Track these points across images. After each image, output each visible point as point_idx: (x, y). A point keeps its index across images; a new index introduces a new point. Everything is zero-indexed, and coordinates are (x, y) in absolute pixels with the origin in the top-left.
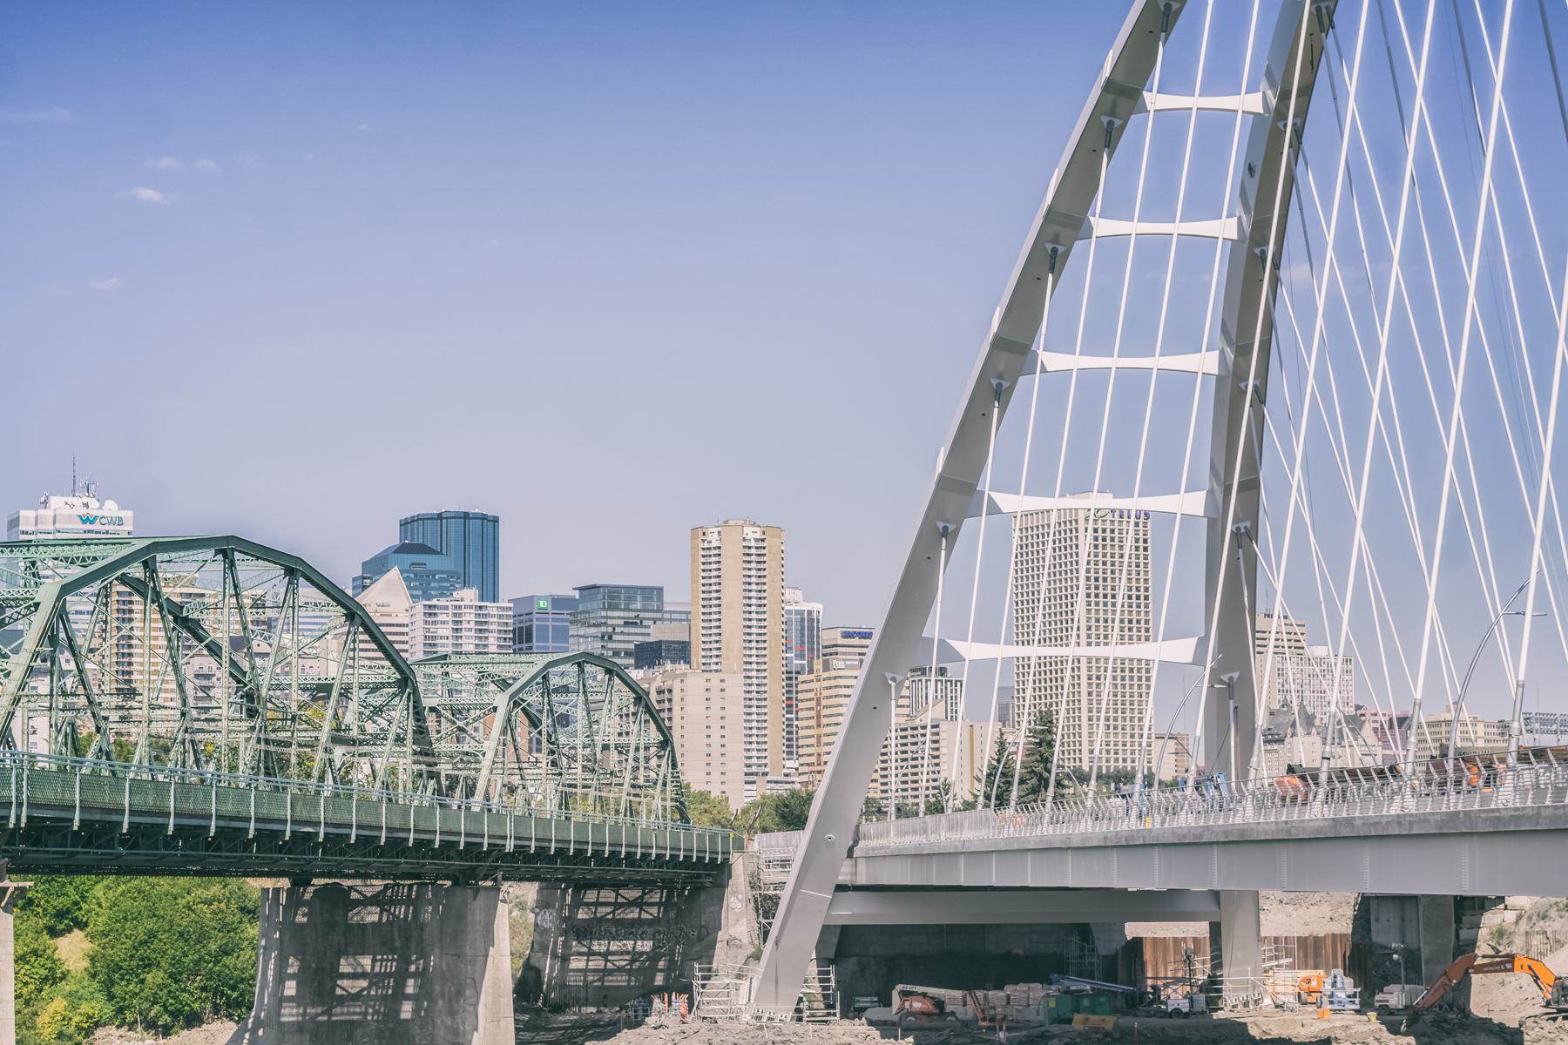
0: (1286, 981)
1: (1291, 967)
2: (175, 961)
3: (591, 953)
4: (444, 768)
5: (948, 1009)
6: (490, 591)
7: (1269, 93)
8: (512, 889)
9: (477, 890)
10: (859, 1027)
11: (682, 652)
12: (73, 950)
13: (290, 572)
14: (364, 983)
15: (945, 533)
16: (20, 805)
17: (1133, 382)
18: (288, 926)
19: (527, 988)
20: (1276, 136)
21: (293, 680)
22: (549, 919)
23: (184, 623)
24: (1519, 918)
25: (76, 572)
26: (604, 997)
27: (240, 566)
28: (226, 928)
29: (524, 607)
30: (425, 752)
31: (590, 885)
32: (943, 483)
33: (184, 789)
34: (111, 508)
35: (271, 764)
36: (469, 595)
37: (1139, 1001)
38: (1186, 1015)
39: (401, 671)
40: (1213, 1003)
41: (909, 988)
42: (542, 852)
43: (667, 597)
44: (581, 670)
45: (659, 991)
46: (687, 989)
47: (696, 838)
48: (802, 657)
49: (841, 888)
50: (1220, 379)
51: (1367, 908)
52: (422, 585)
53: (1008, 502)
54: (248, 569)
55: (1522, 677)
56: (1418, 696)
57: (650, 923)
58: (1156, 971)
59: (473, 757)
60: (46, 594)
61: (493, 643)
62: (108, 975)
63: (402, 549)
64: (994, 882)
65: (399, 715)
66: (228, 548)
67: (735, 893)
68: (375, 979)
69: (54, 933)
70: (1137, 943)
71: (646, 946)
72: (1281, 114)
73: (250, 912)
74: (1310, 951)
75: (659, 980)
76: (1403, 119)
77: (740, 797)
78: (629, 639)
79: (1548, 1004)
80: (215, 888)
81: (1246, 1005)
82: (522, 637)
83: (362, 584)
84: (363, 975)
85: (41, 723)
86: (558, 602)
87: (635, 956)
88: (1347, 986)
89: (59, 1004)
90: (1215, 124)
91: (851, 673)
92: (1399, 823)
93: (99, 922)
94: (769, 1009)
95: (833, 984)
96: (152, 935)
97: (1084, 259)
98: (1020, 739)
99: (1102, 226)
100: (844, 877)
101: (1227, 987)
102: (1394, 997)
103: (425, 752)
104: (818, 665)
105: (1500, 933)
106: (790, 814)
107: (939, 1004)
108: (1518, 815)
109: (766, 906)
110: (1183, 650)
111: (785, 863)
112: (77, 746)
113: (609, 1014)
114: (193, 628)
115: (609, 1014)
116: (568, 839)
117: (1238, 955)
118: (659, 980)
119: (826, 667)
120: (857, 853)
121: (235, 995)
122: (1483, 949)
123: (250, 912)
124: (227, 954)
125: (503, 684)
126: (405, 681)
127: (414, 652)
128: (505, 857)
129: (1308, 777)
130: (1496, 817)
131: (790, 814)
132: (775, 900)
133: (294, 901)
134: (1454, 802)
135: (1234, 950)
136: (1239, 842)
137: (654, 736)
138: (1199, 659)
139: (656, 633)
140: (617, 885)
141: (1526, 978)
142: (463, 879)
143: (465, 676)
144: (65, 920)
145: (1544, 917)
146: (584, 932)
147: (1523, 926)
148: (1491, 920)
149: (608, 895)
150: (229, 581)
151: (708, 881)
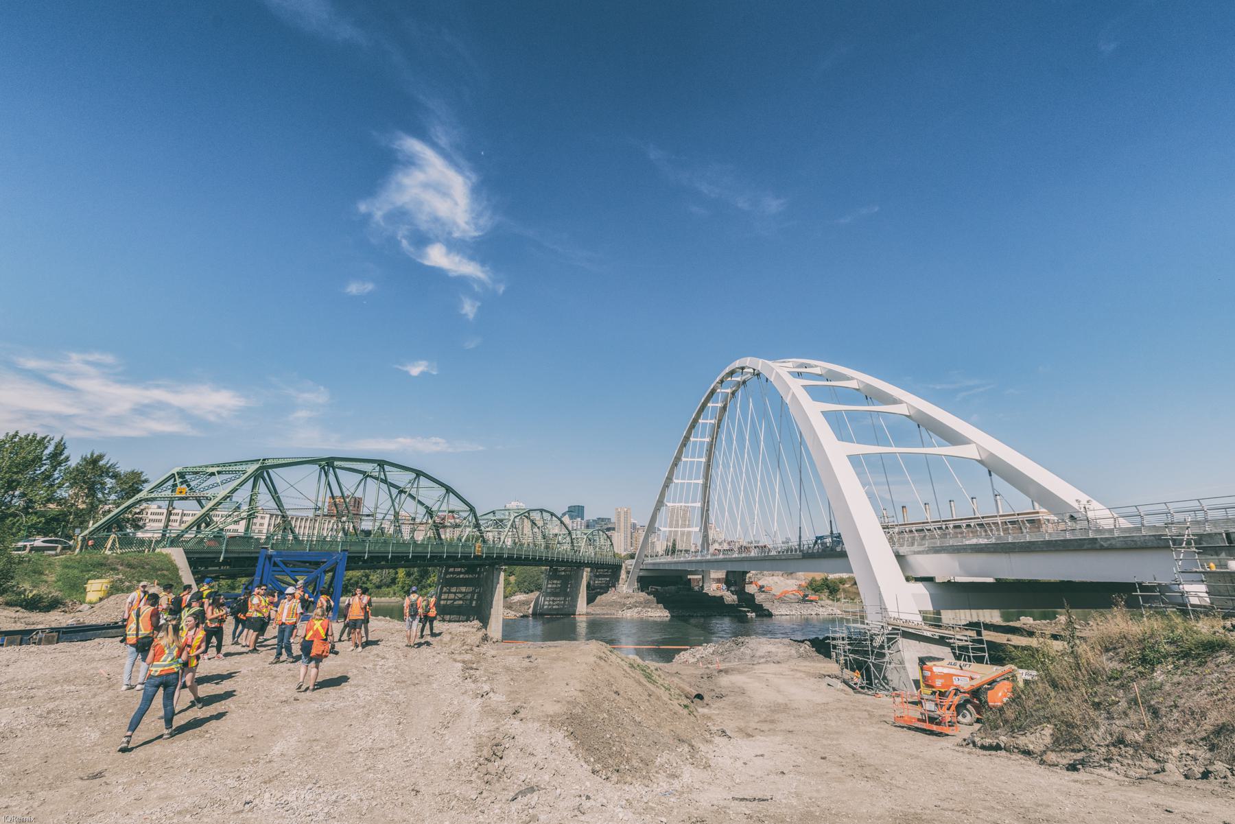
0: (714, 586)
4: (575, 548)
6: (582, 519)
8: (586, 569)
10: (644, 593)
11: (614, 529)
12: (512, 579)
13: (552, 515)
17: (689, 484)
18: (549, 575)
19: (588, 586)
20: (711, 445)
21: (551, 533)
22: (592, 574)
23: (534, 523)
25: (517, 514)
26: (601, 588)
29: (588, 522)
30: (573, 546)
32: (658, 501)
33: (533, 552)
34: (521, 504)
35: (547, 547)
36: (579, 519)
37: (691, 589)
40: (703, 589)
42: (567, 561)
44: (542, 514)
46: (615, 587)
47: (617, 561)
49: (641, 569)
50: (703, 484)
51: (728, 573)
52: (571, 517)
53: (668, 504)
54: (544, 514)
59: (580, 547)
60: (512, 518)
61: (583, 527)
62: (518, 584)
63: (568, 511)
64: (673, 568)
65: (568, 539)
66: (542, 511)
69: (509, 576)
70: (690, 579)
71: (608, 579)
72: (712, 441)
73: (542, 573)
74: (718, 581)
76: (732, 443)
77: (624, 554)
78: (606, 527)
80: (536, 568)
82: (588, 526)
83: (562, 517)
85: (510, 540)
86: (593, 520)
87: (606, 581)
88: (725, 587)
89: (510, 588)
90: (702, 443)
91: (642, 534)
93: (517, 574)
97: (681, 464)
98: (670, 544)
99: (684, 459)
101: (705, 587)
102: (733, 589)
103: (573, 546)
105: (750, 578)
106: (632, 556)
108: (755, 557)
109: (628, 572)
110: (697, 529)
111: (631, 565)
112: (515, 543)
113: (602, 591)
114: (535, 524)
115: (602, 591)
116: (457, 551)
122: (747, 580)
123: (542, 573)
125: (585, 534)
126: (570, 533)
127: (570, 529)
128: (585, 564)
129: (719, 551)
130: (751, 557)
131: (632, 556)
132: (630, 572)
133: (550, 571)
134: (743, 555)
135: (706, 581)
136: (708, 562)
137: (609, 543)
138: (700, 530)
139: (609, 526)
141: (755, 585)
142: (492, 565)
143: (578, 532)
144: (511, 574)
146: (597, 577)
148: (748, 575)
149: (602, 570)
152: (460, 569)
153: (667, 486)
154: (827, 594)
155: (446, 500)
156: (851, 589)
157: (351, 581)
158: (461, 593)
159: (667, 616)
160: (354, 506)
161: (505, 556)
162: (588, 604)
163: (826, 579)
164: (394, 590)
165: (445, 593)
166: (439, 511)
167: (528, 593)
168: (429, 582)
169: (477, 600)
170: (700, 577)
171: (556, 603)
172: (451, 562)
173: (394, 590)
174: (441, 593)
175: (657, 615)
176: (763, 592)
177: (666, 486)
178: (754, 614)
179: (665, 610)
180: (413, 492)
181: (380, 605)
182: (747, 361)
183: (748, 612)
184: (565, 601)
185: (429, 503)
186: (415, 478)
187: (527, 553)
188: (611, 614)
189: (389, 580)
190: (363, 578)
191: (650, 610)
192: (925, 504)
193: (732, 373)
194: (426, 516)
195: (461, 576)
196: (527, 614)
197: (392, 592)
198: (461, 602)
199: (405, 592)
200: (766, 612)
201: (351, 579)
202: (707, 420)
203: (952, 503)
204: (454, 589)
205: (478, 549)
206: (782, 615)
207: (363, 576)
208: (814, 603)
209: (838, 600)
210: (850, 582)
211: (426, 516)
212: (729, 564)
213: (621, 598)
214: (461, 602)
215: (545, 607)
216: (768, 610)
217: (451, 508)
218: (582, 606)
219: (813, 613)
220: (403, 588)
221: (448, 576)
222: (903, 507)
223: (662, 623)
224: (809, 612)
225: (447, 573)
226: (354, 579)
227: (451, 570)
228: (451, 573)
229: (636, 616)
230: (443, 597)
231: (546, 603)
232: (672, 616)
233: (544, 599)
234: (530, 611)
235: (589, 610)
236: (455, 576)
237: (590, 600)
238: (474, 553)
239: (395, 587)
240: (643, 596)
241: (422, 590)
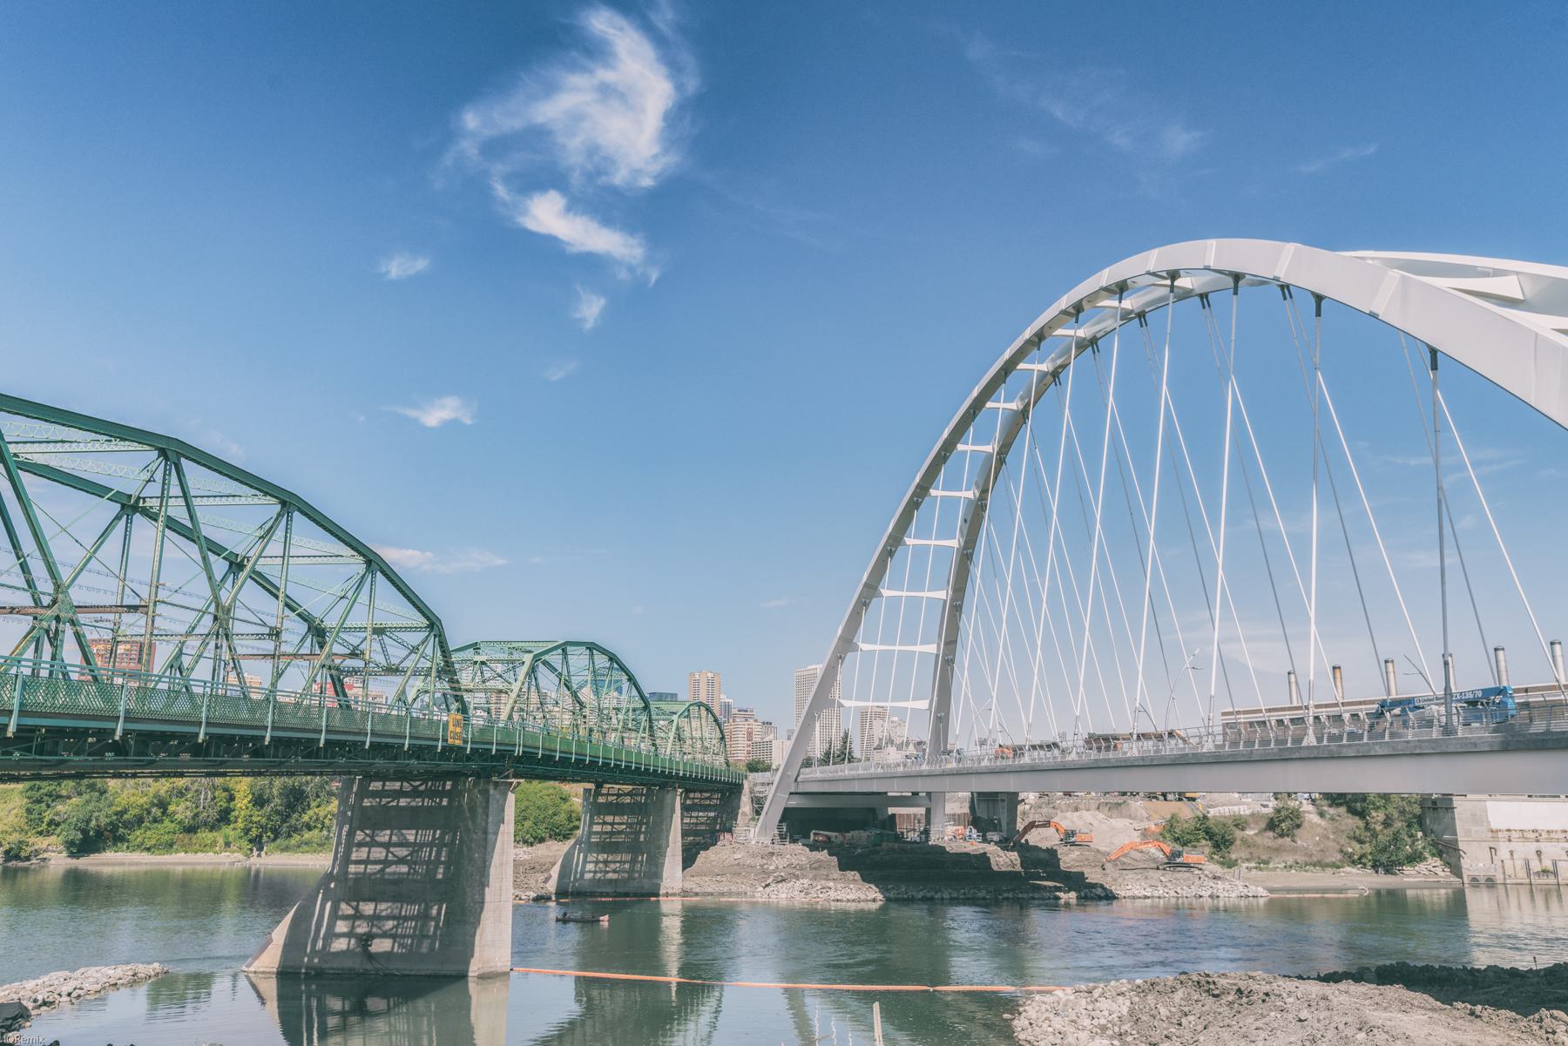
0: (951, 829)
1: (954, 825)
2: (536, 818)
3: (691, 817)
5: (832, 840)
7: (976, 491)
9: (668, 791)
10: (798, 847)
14: (624, 827)
15: (840, 657)
16: (520, 746)
24: (1031, 808)
27: (595, 657)
28: (555, 805)
31: (691, 792)
38: (918, 843)
39: (645, 703)
41: (817, 832)
43: (679, 696)
45: (718, 831)
48: (725, 717)
49: (791, 794)
55: (1030, 721)
56: (1078, 714)
57: (713, 806)
58: (901, 827)
66: (591, 647)
67: (745, 795)
68: (629, 825)
70: (893, 816)
71: (712, 814)
74: (956, 819)
75: (718, 827)
79: (1062, 840)
81: (938, 839)
84: (623, 824)
87: (709, 818)
88: (974, 833)
92: (1143, 760)
94: (762, 839)
95: (785, 830)
96: (527, 808)
100: (793, 791)
104: (731, 720)
107: (829, 838)
110: (923, 704)
117: (936, 820)
118: (718, 827)
119: (734, 721)
120: (799, 779)
121: (558, 831)
124: (555, 815)
135: (934, 819)
140: (701, 792)
145: (1040, 807)
147: (1033, 811)
149: (698, 795)
150: (591, 662)
151: (735, 790)
152: (399, 784)
153: (866, 605)
154: (1207, 850)
155: (364, 597)
156: (1259, 840)
157: (126, 817)
158: (403, 844)
159: (874, 900)
160: (140, 660)
161: (518, 751)
162: (684, 869)
163: (1205, 817)
164: (226, 837)
165: (360, 845)
166: (342, 628)
167: (532, 844)
168: (306, 818)
169: (448, 864)
170: (922, 811)
171: (613, 866)
172: (380, 763)
173: (226, 837)
174: (350, 844)
175: (851, 897)
176: (1073, 844)
177: (863, 603)
178: (1073, 895)
179: (867, 885)
180: (269, 567)
181: (194, 871)
182: (1155, 259)
183: (1058, 889)
184: (633, 862)
185: (314, 604)
186: (279, 515)
187: (565, 748)
188: (738, 894)
189: (213, 814)
190: (154, 810)
191: (831, 884)
192: (1552, 644)
193: (1121, 289)
194: (309, 640)
195: (403, 802)
196: (543, 892)
197: (221, 841)
198: (404, 869)
199: (250, 841)
200: (1099, 891)
201: (125, 811)
202: (972, 451)
203: (1557, 647)
204: (384, 836)
205: (452, 729)
206: (1134, 898)
207: (153, 805)
208: (1197, 872)
209: (1231, 864)
210: (1257, 823)
211: (309, 640)
212: (973, 778)
213: (754, 856)
214: (404, 869)
215: (588, 876)
216: (1102, 886)
217: (382, 620)
218: (672, 875)
219: (1203, 893)
220: (247, 831)
221: (367, 803)
222: (1334, 668)
223: (861, 916)
224: (1194, 890)
225: (364, 793)
226: (133, 812)
227: (376, 786)
228: (375, 794)
229: (800, 900)
230: (354, 856)
231: (590, 867)
232: (888, 900)
233: (585, 858)
234: (551, 887)
235: (689, 885)
236: (384, 801)
237: (688, 860)
238: (445, 740)
239: (228, 831)
240: (798, 853)
241: (290, 836)
